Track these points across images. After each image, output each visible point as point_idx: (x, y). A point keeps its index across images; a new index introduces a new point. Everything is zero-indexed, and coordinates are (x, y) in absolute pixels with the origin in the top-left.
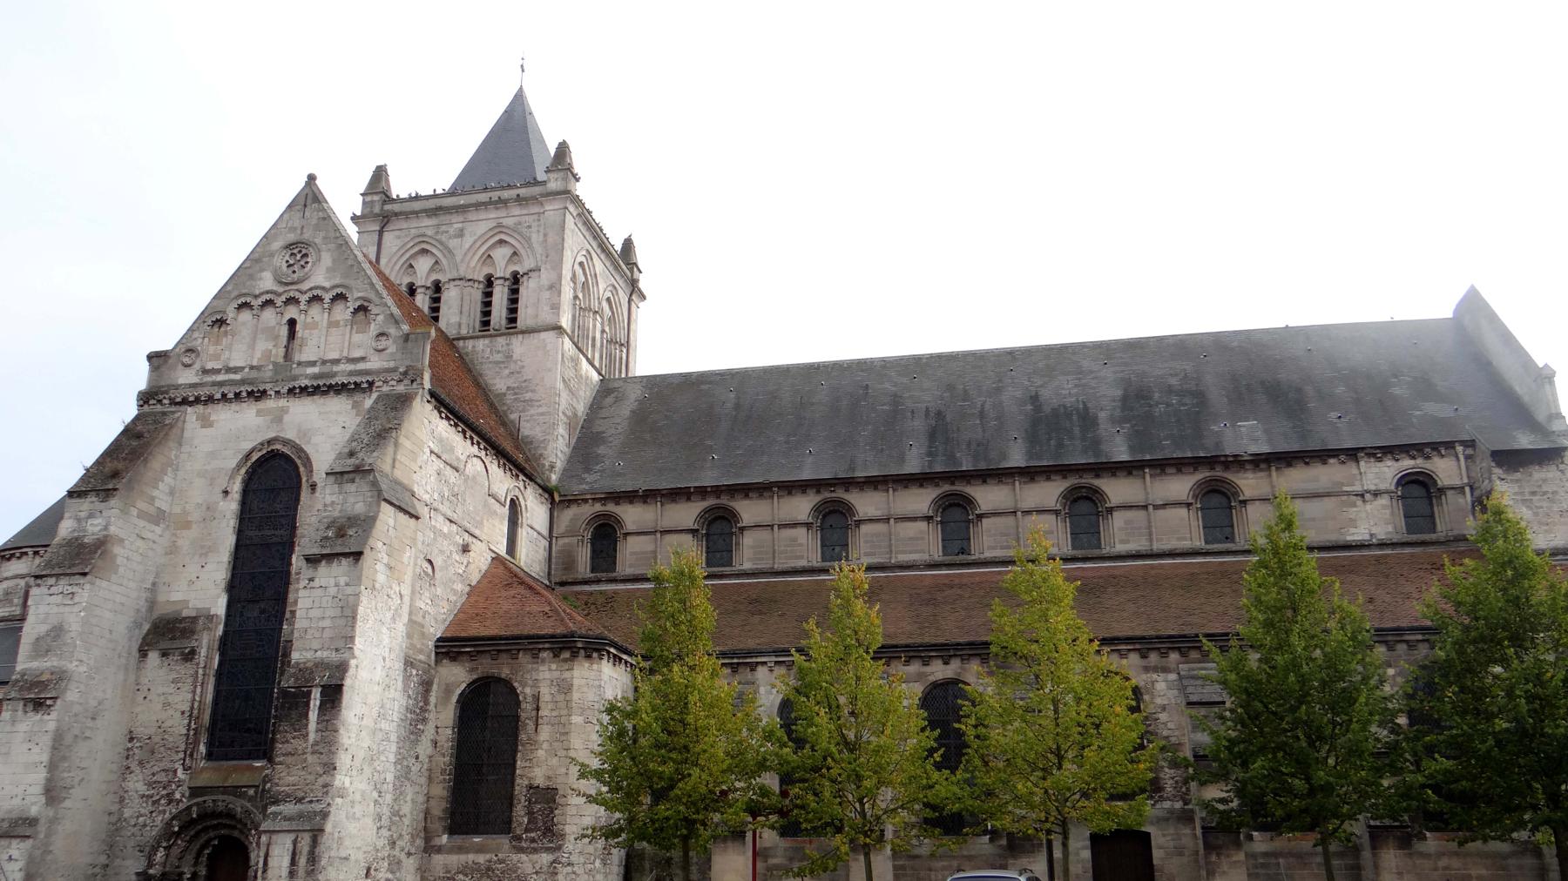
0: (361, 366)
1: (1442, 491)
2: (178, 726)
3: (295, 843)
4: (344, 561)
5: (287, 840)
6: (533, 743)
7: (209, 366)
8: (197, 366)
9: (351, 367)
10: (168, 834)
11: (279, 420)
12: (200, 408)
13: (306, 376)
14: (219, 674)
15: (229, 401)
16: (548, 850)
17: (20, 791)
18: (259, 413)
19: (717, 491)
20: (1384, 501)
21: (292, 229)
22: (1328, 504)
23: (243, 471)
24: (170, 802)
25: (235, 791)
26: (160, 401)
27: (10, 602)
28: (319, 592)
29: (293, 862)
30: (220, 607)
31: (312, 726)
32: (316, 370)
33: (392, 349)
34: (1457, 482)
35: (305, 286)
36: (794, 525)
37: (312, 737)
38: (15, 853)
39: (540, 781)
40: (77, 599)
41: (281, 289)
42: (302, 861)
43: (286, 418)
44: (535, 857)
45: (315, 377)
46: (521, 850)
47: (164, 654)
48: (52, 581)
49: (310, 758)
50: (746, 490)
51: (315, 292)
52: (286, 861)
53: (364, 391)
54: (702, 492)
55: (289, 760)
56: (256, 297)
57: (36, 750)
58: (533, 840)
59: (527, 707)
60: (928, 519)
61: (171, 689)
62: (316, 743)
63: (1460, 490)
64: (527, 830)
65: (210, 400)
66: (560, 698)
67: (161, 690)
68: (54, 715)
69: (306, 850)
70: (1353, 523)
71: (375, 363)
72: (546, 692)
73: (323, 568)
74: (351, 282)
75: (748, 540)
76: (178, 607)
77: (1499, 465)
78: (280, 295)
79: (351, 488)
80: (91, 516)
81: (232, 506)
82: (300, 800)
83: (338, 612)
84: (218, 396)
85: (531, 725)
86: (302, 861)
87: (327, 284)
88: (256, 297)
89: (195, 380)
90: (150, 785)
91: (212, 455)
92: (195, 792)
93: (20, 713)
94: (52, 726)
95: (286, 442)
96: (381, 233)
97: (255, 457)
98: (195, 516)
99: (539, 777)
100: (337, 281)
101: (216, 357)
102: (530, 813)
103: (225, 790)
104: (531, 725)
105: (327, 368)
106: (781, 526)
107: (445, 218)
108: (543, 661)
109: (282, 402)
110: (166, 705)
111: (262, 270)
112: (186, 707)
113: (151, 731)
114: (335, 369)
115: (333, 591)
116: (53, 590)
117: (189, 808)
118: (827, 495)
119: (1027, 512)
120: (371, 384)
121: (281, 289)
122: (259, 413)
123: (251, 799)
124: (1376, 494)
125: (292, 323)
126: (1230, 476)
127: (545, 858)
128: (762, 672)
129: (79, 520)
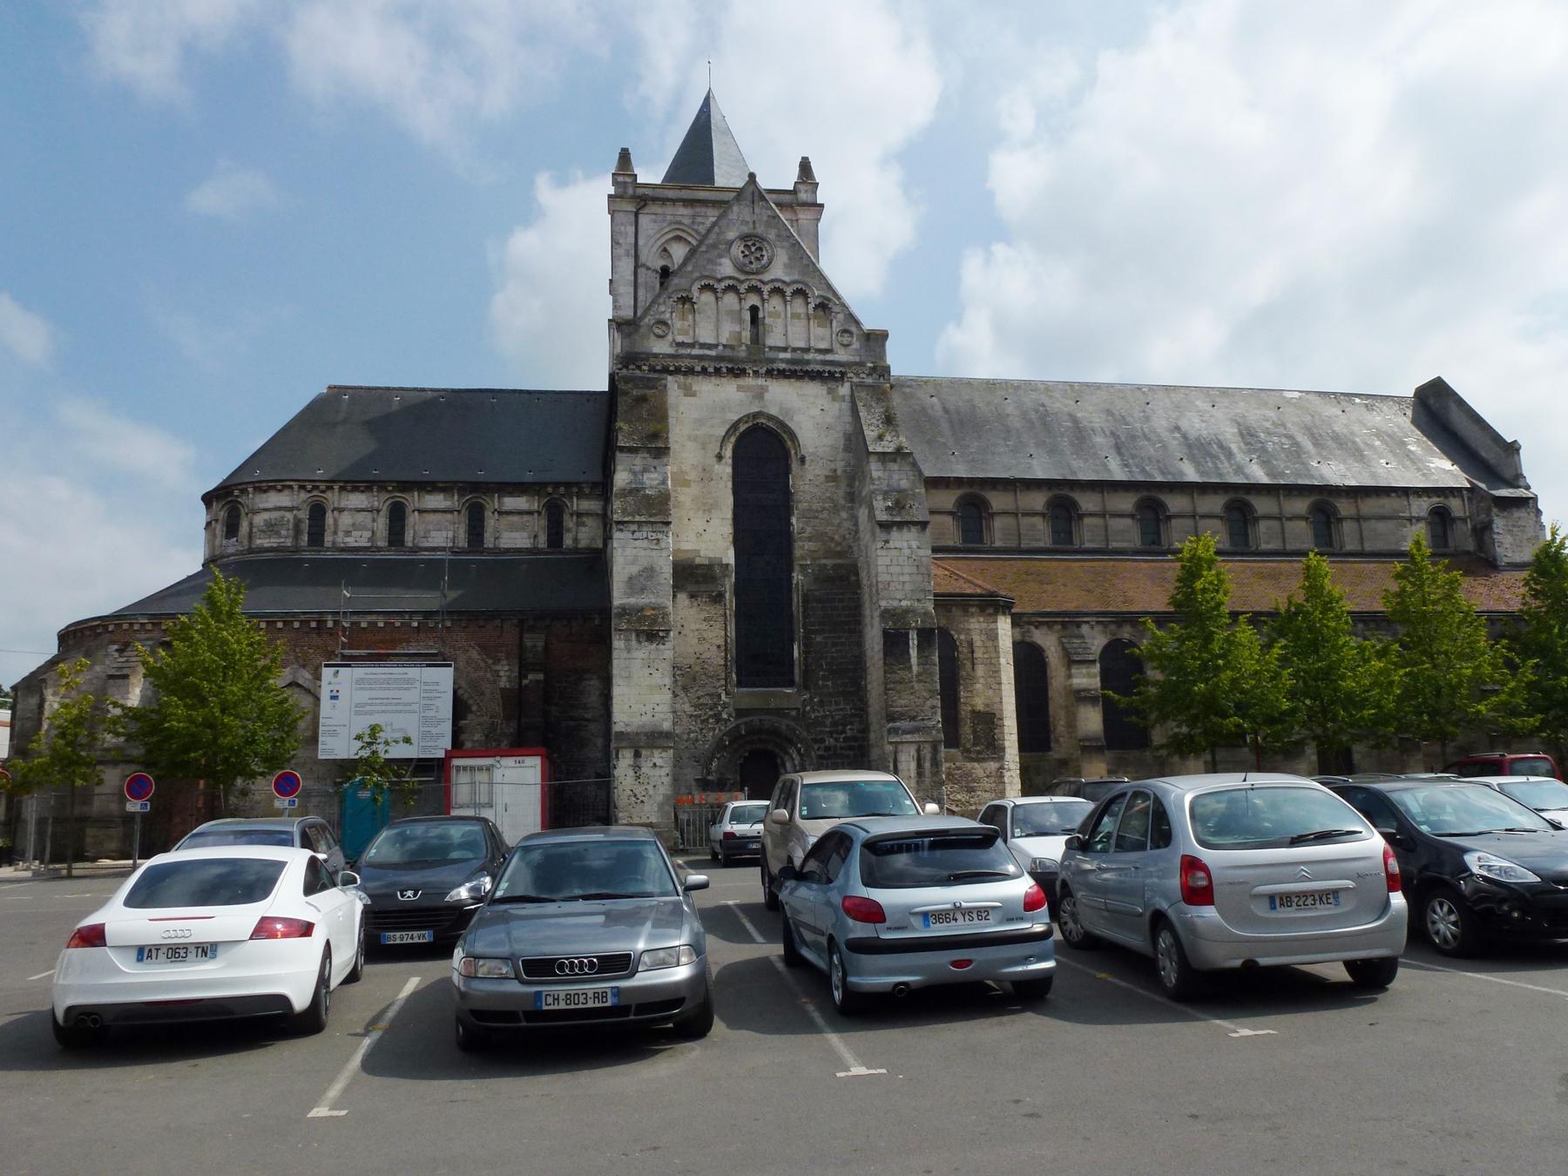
0: (829, 357)
1: (1454, 520)
2: (716, 658)
3: (918, 751)
4: (913, 529)
5: (912, 750)
6: (972, 678)
7: (680, 339)
8: (670, 338)
9: (820, 357)
10: (719, 746)
11: (760, 395)
12: (681, 378)
13: (782, 360)
14: (737, 615)
15: (710, 375)
16: (993, 759)
17: (648, 708)
18: (740, 388)
19: (971, 482)
20: (1422, 525)
21: (745, 223)
22: (1391, 524)
23: (733, 439)
24: (717, 722)
25: (779, 712)
26: (639, 368)
27: (278, 534)
28: (894, 552)
29: (919, 765)
30: (730, 557)
31: (914, 660)
32: (788, 355)
33: (856, 345)
34: (1461, 514)
35: (766, 277)
36: (1034, 514)
37: (915, 668)
38: (659, 762)
39: (980, 707)
40: (663, 545)
41: (742, 277)
42: (927, 765)
43: (767, 396)
44: (985, 765)
45: (788, 361)
46: (973, 760)
47: (692, 596)
48: (634, 527)
49: (916, 686)
50: (994, 483)
51: (777, 285)
52: (913, 766)
53: (836, 380)
54: (959, 482)
55: (898, 687)
56: (719, 281)
57: (657, 675)
58: (979, 752)
59: (964, 650)
60: (1132, 516)
61: (704, 626)
62: (919, 674)
63: (1464, 520)
64: (974, 745)
65: (690, 372)
66: (989, 644)
67: (693, 627)
68: (669, 645)
69: (928, 756)
70: (1404, 538)
71: (841, 356)
72: (978, 640)
73: (895, 534)
74: (807, 279)
75: (998, 523)
76: (690, 555)
77: (1497, 505)
78: (742, 282)
79: (895, 467)
80: (645, 470)
81: (726, 469)
82: (913, 718)
83: (914, 570)
84: (698, 369)
85: (968, 665)
86: (927, 765)
87: (787, 279)
88: (788, 284)
89: (671, 351)
90: (696, 706)
91: (700, 422)
92: (740, 713)
93: (634, 642)
94: (669, 654)
95: (771, 418)
96: (636, 215)
97: (743, 428)
98: (692, 476)
99: (979, 703)
100: (796, 277)
101: (684, 332)
102: (974, 732)
103: (768, 711)
104: (968, 665)
105: (798, 355)
106: (1025, 515)
107: (700, 210)
108: (972, 615)
109: (761, 381)
110: (702, 640)
111: (720, 256)
112: (721, 642)
113: (692, 661)
114: (806, 357)
115: (907, 552)
116: (637, 535)
117: (738, 726)
118: (1057, 492)
119: (1203, 517)
120: (843, 374)
121: (742, 277)
122: (740, 388)
123: (794, 719)
124: (1419, 519)
125: (754, 310)
126: (1331, 500)
127: (993, 766)
128: (1085, 629)
129: (634, 473)
